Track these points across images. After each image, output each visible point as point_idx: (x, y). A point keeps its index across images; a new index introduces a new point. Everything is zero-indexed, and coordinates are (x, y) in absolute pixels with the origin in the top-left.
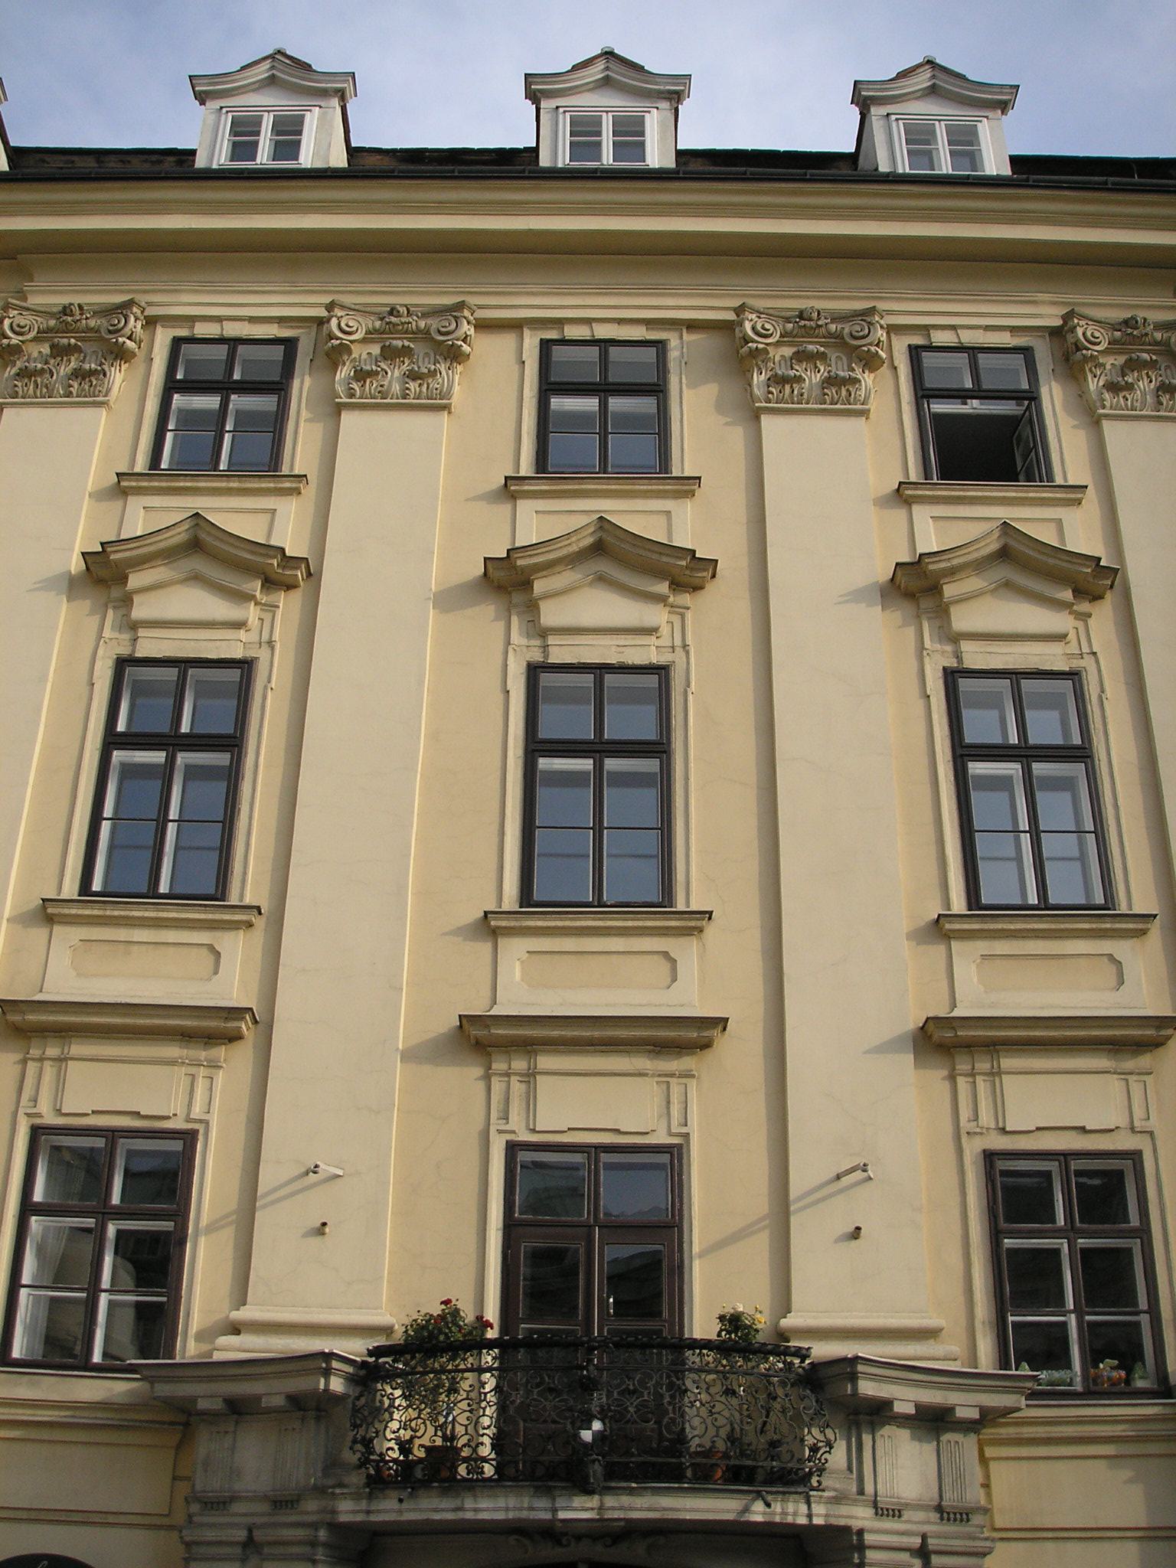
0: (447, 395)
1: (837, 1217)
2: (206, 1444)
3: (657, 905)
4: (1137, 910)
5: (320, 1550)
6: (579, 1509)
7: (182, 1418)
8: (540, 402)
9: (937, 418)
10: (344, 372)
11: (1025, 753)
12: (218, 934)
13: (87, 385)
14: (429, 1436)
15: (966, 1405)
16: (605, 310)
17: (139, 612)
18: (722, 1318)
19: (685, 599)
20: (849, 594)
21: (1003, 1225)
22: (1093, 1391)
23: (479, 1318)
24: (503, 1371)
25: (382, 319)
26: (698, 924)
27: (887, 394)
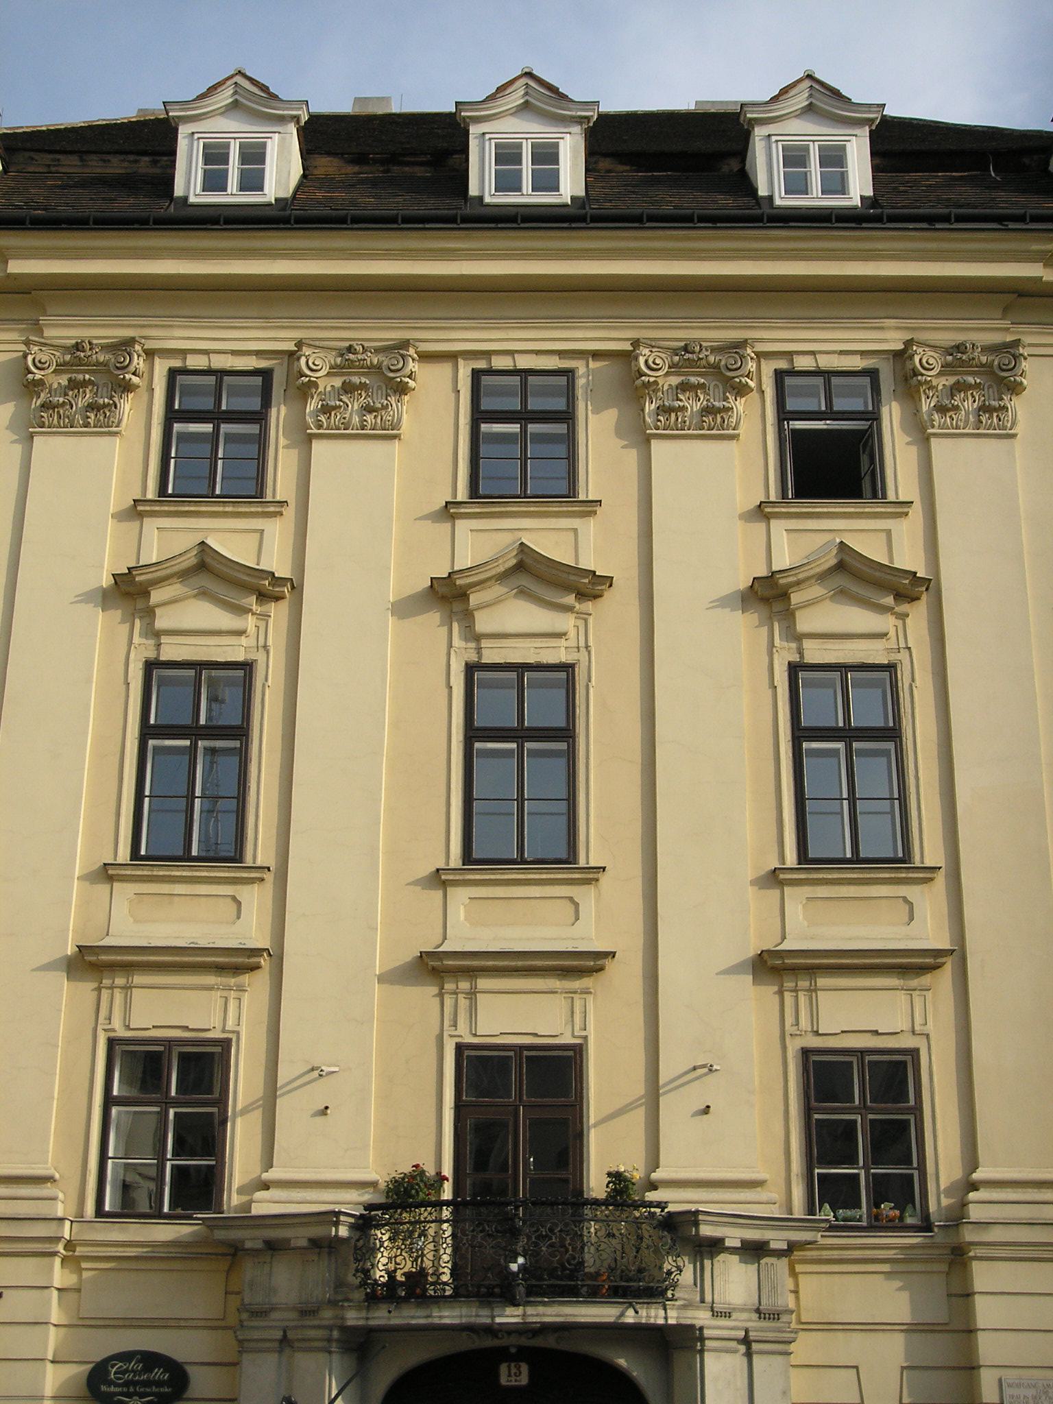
0: (396, 425)
1: (695, 1095)
2: (249, 1270)
3: (563, 858)
4: (928, 863)
5: (334, 1344)
6: (510, 1316)
7: (232, 1251)
8: (472, 428)
9: (795, 432)
10: (312, 405)
11: (847, 734)
12: (239, 887)
13: (100, 418)
14: (407, 1266)
15: (777, 1239)
16: (526, 343)
17: (160, 624)
18: (609, 1174)
19: (588, 606)
20: (717, 600)
21: (814, 1104)
22: (877, 1225)
23: (439, 1174)
24: (455, 1222)
25: (342, 355)
26: (595, 876)
27: (754, 418)
